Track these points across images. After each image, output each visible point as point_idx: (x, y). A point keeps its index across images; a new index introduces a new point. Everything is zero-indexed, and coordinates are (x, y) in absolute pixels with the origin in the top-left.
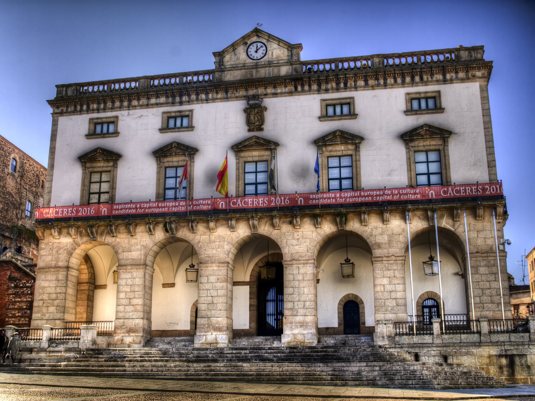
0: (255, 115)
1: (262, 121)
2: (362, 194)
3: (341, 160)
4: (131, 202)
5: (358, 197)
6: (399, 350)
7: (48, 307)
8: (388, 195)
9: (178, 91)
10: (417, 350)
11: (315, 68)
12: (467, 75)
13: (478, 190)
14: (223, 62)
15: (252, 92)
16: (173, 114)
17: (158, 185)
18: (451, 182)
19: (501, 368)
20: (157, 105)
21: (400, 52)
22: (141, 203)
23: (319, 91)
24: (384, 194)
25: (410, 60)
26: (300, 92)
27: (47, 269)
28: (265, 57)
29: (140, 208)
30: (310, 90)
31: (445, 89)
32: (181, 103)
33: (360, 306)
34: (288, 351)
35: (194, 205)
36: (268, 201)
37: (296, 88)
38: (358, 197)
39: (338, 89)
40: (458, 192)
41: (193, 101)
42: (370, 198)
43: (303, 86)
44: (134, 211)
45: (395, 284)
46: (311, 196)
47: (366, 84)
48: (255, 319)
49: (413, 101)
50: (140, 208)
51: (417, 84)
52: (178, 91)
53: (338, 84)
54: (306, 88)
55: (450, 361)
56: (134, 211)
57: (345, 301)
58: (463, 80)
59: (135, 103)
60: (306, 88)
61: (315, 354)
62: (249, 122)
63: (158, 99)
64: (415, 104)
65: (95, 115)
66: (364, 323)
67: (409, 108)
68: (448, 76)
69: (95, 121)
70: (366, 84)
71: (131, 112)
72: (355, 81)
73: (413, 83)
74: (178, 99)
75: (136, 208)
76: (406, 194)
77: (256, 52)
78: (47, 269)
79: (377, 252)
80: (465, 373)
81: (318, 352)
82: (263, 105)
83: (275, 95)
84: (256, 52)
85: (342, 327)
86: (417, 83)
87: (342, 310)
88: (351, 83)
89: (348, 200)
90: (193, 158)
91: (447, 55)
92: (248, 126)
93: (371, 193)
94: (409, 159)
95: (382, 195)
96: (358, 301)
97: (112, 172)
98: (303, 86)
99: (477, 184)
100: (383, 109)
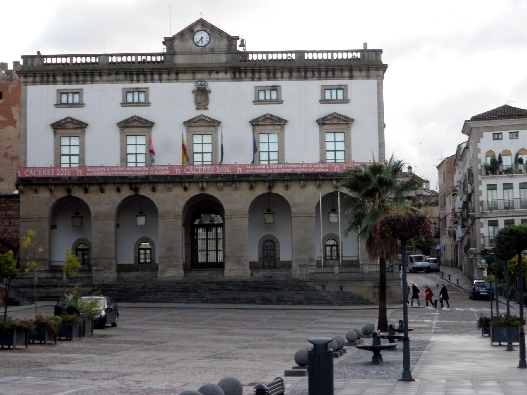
0: (202, 94)
2: (286, 166)
3: (137, 139)
4: (102, 167)
5: (282, 168)
6: (313, 283)
8: (305, 168)
10: (324, 283)
12: (34, 80)
13: (51, 173)
14: (173, 46)
15: (199, 76)
16: (132, 90)
18: (284, 160)
19: (375, 294)
21: (111, 53)
22: (110, 167)
23: (253, 79)
24: (302, 167)
26: (238, 79)
28: (209, 45)
29: (270, 168)
30: (246, 77)
32: (138, 81)
33: (276, 245)
34: (241, 284)
36: (54, 172)
38: (282, 168)
40: (37, 173)
41: (37, 82)
44: (105, 173)
46: (247, 167)
49: (260, 92)
50: (270, 168)
55: (344, 290)
56: (105, 173)
61: (260, 286)
62: (197, 103)
63: (118, 76)
66: (279, 258)
67: (257, 99)
73: (327, 78)
75: (107, 171)
76: (318, 168)
77: (202, 38)
79: (294, 210)
80: (352, 297)
81: (261, 284)
82: (207, 88)
83: (218, 80)
84: (202, 38)
86: (156, 80)
88: (279, 75)
89: (275, 171)
90: (350, 127)
92: (196, 105)
93: (293, 166)
95: (300, 168)
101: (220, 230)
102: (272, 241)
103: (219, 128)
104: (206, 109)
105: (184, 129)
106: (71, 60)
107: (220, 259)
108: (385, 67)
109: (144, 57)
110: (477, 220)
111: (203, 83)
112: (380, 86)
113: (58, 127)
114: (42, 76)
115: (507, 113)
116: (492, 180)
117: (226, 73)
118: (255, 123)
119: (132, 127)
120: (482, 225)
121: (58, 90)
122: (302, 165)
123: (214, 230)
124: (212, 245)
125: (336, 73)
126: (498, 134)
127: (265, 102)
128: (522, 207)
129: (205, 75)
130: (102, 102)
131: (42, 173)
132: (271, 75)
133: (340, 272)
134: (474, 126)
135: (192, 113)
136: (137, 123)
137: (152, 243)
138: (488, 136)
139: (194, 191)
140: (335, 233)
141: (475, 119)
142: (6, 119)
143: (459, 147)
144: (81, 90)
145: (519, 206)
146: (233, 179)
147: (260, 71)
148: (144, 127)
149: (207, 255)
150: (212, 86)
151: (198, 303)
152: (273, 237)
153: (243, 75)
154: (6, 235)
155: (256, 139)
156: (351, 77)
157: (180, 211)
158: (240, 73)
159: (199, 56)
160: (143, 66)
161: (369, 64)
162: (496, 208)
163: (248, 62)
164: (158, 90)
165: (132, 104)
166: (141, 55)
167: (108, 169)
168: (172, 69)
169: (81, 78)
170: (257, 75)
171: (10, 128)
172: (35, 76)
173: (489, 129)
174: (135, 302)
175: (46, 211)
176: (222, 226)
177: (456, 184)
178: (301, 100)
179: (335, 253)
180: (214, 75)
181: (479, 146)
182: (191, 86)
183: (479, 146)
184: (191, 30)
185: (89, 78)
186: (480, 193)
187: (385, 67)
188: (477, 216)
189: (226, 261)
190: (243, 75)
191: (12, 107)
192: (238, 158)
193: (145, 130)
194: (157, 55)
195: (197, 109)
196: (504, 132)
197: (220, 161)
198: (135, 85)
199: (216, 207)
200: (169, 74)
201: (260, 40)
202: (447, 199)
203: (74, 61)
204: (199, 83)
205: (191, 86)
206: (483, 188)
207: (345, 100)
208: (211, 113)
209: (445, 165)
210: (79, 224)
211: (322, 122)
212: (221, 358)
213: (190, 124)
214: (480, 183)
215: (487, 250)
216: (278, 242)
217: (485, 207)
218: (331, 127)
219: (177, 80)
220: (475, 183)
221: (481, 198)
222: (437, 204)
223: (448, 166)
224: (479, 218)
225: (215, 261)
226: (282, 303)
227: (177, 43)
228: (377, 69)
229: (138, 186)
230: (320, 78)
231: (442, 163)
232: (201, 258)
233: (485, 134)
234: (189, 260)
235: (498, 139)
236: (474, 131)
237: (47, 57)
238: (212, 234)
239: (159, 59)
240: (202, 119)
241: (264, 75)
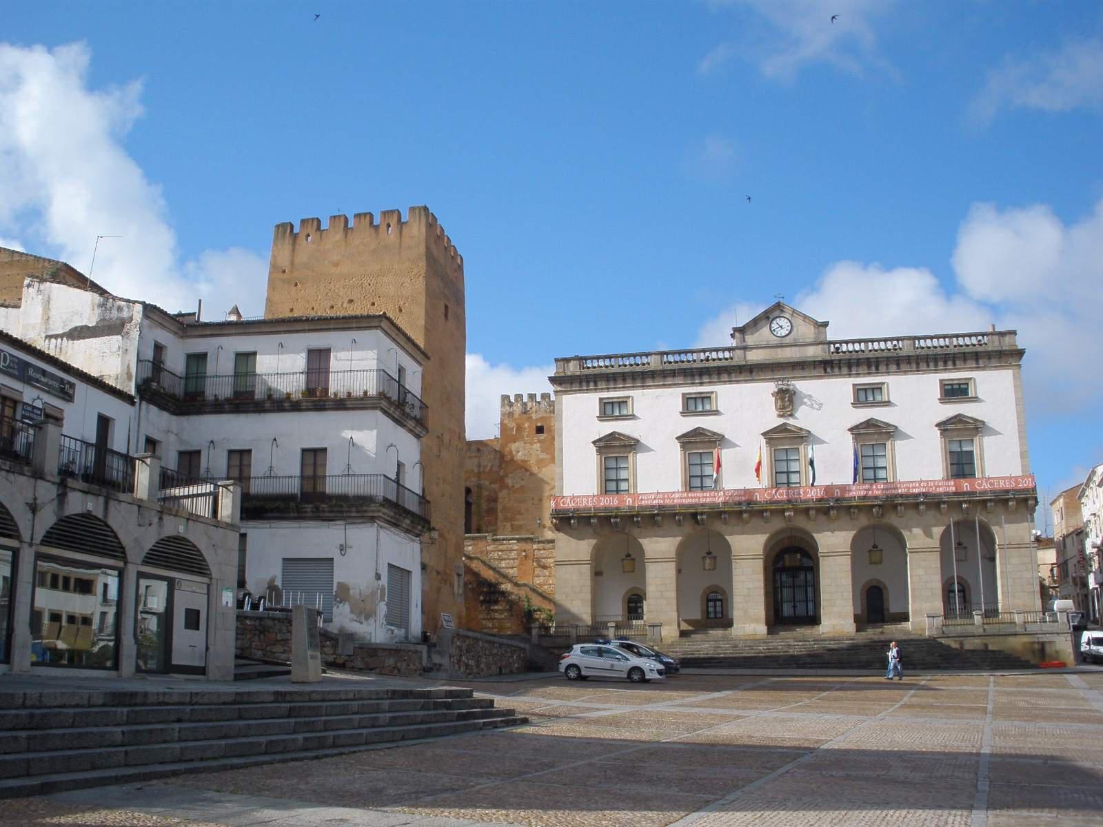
7: (572, 600)
9: (699, 373)
11: (844, 347)
16: (694, 396)
21: (932, 334)
23: (850, 375)
32: (701, 384)
33: (884, 591)
35: (936, 487)
42: (697, 500)
43: (832, 368)
52: (867, 362)
57: (868, 586)
64: (862, 398)
65: (605, 395)
66: (888, 610)
69: (606, 401)
75: (663, 499)
87: (865, 597)
96: (881, 586)
99: (1011, 478)
100: (914, 400)
106: (867, 347)
122: (920, 484)
125: (958, 362)
131: (999, 485)
133: (983, 624)
135: (773, 420)
139: (777, 524)
140: (639, 586)
149: (795, 607)
151: (793, 668)
153: (836, 370)
158: (832, 368)
163: (841, 354)
164: (726, 394)
167: (666, 496)
174: (705, 667)
179: (719, 609)
182: (771, 387)
190: (836, 370)
195: (780, 416)
197: (811, 482)
205: (771, 387)
212: (247, 767)
216: (886, 588)
225: (804, 613)
226: (910, 667)
230: (936, 370)
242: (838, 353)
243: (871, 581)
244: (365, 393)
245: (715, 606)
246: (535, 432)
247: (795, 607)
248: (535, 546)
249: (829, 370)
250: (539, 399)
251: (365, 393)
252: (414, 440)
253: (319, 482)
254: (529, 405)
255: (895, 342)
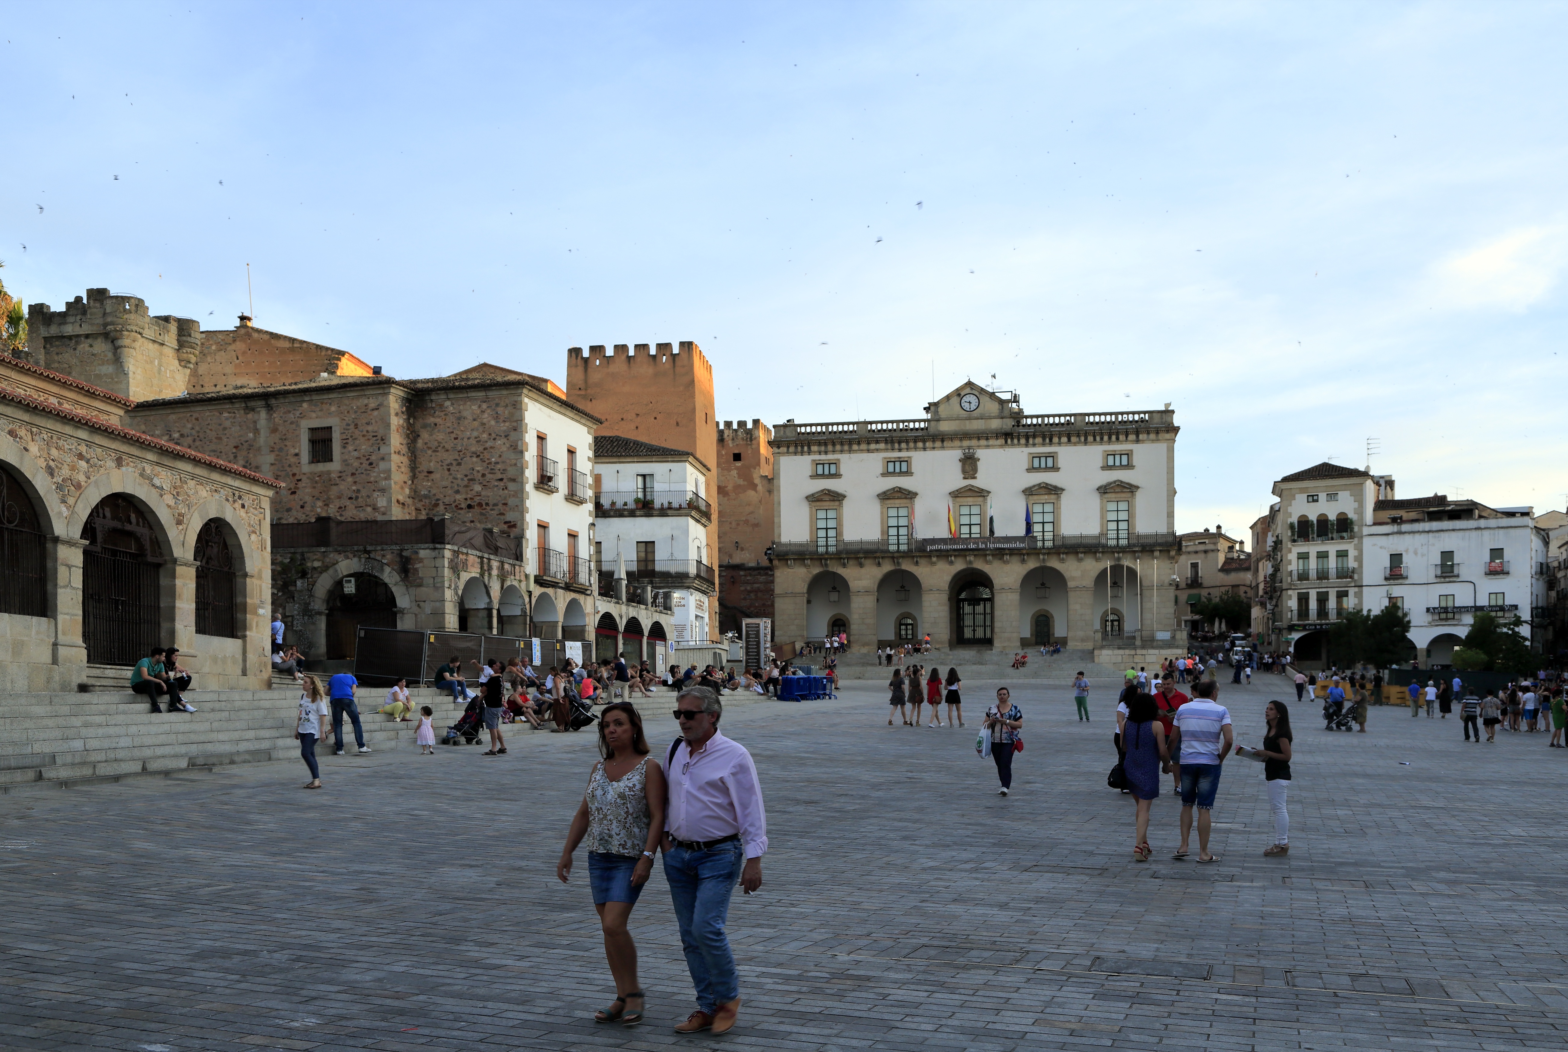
0: (969, 464)
1: (975, 470)
15: (966, 443)
17: (882, 523)
20: (877, 450)
23: (1027, 445)
25: (1108, 418)
27: (785, 595)
30: (1019, 444)
31: (1135, 447)
32: (900, 450)
37: (1006, 442)
39: (1044, 445)
43: (1012, 439)
45: (127, 735)
47: (1069, 440)
48: (776, 526)
51: (1113, 443)
53: (1044, 440)
54: (1016, 441)
58: (1153, 441)
59: (855, 447)
60: (1016, 441)
62: (964, 471)
68: (1141, 437)
70: (1069, 440)
71: (852, 455)
72: (1060, 438)
74: (896, 446)
78: (785, 595)
79: (1071, 584)
83: (988, 447)
85: (1034, 639)
88: (1056, 440)
91: (1142, 415)
94: (1102, 509)
97: (838, 509)
98: (1012, 439)
101: (988, 605)
102: (1046, 616)
103: (989, 498)
104: (975, 478)
105: (950, 499)
106: (827, 429)
107: (988, 635)
108: (1176, 430)
109: (906, 424)
110: (1284, 592)
111: (971, 451)
112: (1171, 451)
113: (814, 499)
114: (796, 446)
115: (1326, 471)
116: (1302, 547)
117: (997, 439)
118: (1029, 492)
119: (894, 498)
120: (1290, 597)
121: (813, 461)
123: (982, 606)
124: (980, 619)
126: (1313, 496)
127: (1039, 469)
128: (1337, 578)
129: (974, 442)
130: (861, 475)
132: (1047, 440)
134: (1286, 485)
135: (959, 482)
136: (899, 495)
137: (914, 619)
138: (1302, 498)
139: (959, 565)
141: (1286, 479)
142: (746, 483)
143: (1272, 507)
144: (839, 460)
145: (1335, 576)
146: (1004, 551)
147: (1034, 437)
148: (906, 498)
149: (974, 630)
150: (980, 453)
152: (1047, 611)
154: (752, 609)
155: (1030, 510)
156: (1138, 441)
157: (946, 586)
159: (967, 422)
160: (905, 434)
161: (1159, 426)
162: (1307, 579)
165: (894, 474)
166: (903, 421)
168: (936, 436)
169: (838, 447)
170: (1031, 441)
171: (751, 493)
172: (788, 447)
173: (1302, 490)
175: (803, 587)
176: (991, 600)
177: (1269, 549)
178: (1080, 468)
179: (910, 632)
180: (983, 442)
181: (1290, 509)
183: (1290, 509)
184: (958, 393)
185: (846, 447)
186: (1290, 562)
187: (1176, 430)
188: (1284, 587)
189: (995, 636)
191: (752, 470)
192: (1009, 525)
193: (907, 501)
194: (920, 421)
195: (964, 478)
196: (1320, 494)
198: (896, 454)
199: (985, 581)
200: (934, 441)
201: (1036, 404)
202: (1261, 564)
203: (830, 430)
204: (967, 451)
205: (958, 454)
206: (1293, 556)
207: (1129, 466)
208: (980, 482)
209: (1259, 525)
210: (836, 599)
211: (1104, 490)
213: (956, 495)
214: (1290, 551)
215: (1295, 625)
217: (1295, 577)
218: (1113, 495)
219: (943, 448)
220: (1284, 551)
221: (1290, 568)
222: (1248, 569)
223: (1262, 527)
224: (1287, 589)
227: (943, 411)
228: (1168, 431)
229: (900, 560)
231: (1255, 524)
232: (968, 634)
233: (1297, 496)
234: (955, 636)
235: (1314, 501)
236: (1284, 493)
237: (801, 426)
238: (980, 609)
239: (922, 425)
240: (970, 489)
241: (1039, 440)
242: (1018, 426)
243: (1034, 615)
244: (680, 505)
245: (907, 630)
246: (732, 458)
247: (974, 630)
248: (742, 573)
249: (1009, 441)
250: (735, 426)
251: (680, 505)
252: (702, 528)
253: (650, 564)
254: (726, 433)
255: (1068, 418)
